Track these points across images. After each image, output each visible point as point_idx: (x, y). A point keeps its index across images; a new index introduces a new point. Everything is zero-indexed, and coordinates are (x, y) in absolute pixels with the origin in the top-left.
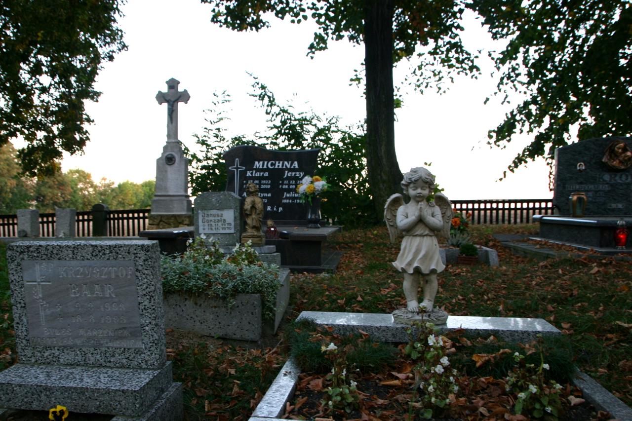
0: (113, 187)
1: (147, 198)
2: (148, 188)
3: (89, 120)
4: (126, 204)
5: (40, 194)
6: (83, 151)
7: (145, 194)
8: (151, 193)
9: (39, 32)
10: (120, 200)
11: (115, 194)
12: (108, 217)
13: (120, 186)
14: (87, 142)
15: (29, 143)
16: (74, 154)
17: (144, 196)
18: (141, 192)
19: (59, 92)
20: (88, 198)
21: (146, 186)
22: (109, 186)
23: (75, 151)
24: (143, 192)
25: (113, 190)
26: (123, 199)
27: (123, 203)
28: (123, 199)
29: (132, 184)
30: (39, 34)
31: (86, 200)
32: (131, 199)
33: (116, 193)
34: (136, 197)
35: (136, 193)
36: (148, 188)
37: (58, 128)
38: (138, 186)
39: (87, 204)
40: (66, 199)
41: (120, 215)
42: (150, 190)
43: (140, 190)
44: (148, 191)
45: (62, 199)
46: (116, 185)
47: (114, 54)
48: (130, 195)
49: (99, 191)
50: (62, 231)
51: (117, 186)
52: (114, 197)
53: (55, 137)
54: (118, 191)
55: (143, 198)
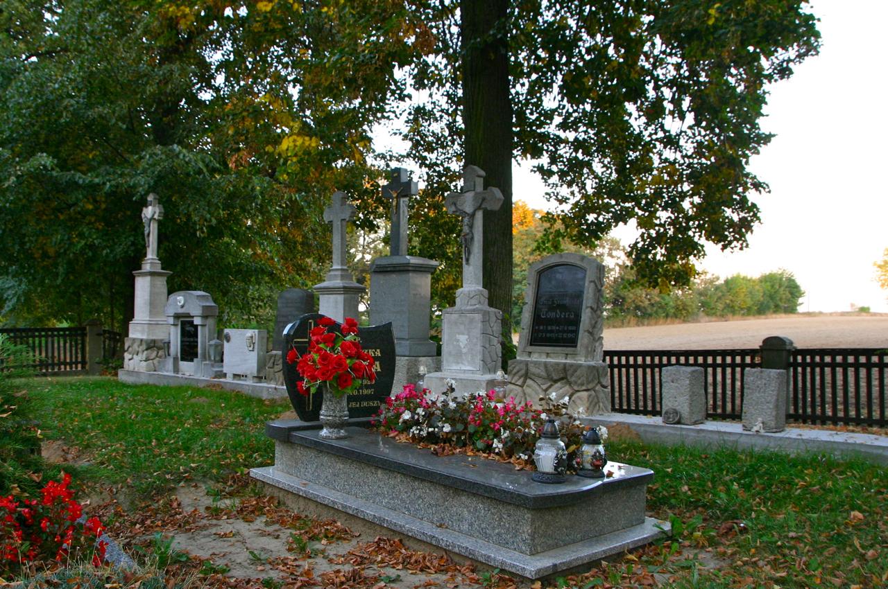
0: (717, 283)
1: (768, 299)
2: (768, 284)
3: (757, 186)
4: (736, 308)
5: (619, 296)
6: (745, 241)
7: (764, 294)
8: (773, 291)
9: (709, 7)
10: (728, 301)
11: (720, 294)
12: (791, 359)
13: (727, 282)
14: (755, 225)
15: (643, 230)
16: (729, 249)
17: (763, 296)
18: (758, 291)
19: (692, 142)
20: (682, 301)
21: (766, 281)
22: (712, 282)
23: (730, 242)
24: (761, 290)
25: (717, 288)
26: (731, 301)
27: (733, 307)
28: (731, 301)
29: (744, 278)
30: (712, 12)
31: (679, 303)
32: (745, 302)
33: (722, 291)
34: (752, 298)
35: (751, 293)
36: (768, 284)
37: (692, 203)
38: (754, 281)
39: (681, 308)
40: (653, 301)
41: (817, 359)
42: (772, 286)
43: (757, 287)
44: (769, 288)
45: (647, 302)
46: (721, 281)
47: (791, 65)
48: (742, 295)
49: (698, 289)
50: (760, 419)
51: (723, 282)
52: (720, 298)
53: (688, 218)
54: (724, 289)
55: (762, 299)
